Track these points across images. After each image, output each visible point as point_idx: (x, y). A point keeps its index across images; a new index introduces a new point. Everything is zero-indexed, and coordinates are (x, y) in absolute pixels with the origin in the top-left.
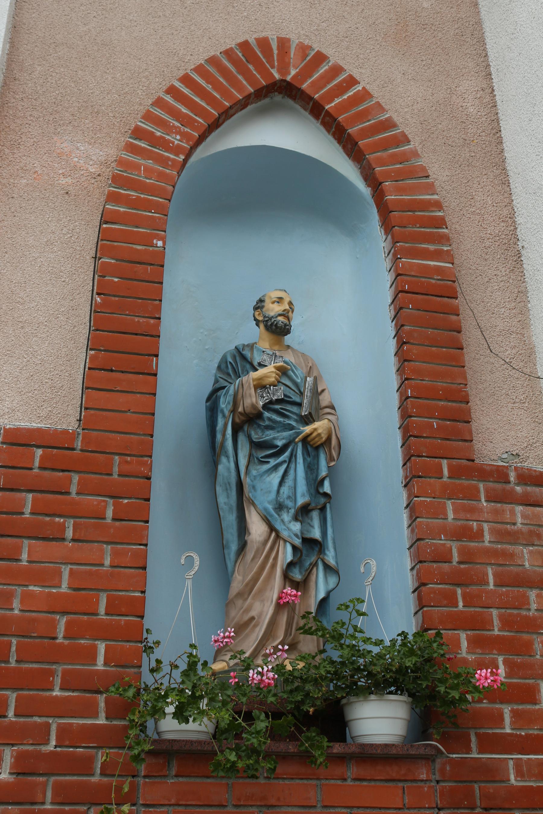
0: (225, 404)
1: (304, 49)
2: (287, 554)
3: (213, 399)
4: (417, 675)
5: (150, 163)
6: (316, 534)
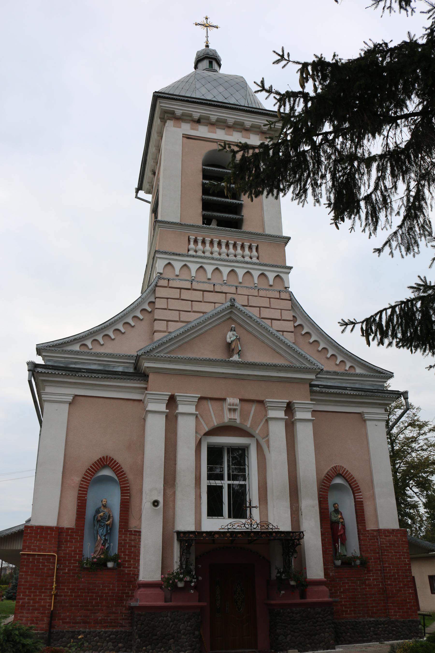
0: (96, 519)
1: (110, 458)
2: (102, 542)
3: (94, 517)
4: (114, 559)
5: (85, 483)
6: (107, 538)
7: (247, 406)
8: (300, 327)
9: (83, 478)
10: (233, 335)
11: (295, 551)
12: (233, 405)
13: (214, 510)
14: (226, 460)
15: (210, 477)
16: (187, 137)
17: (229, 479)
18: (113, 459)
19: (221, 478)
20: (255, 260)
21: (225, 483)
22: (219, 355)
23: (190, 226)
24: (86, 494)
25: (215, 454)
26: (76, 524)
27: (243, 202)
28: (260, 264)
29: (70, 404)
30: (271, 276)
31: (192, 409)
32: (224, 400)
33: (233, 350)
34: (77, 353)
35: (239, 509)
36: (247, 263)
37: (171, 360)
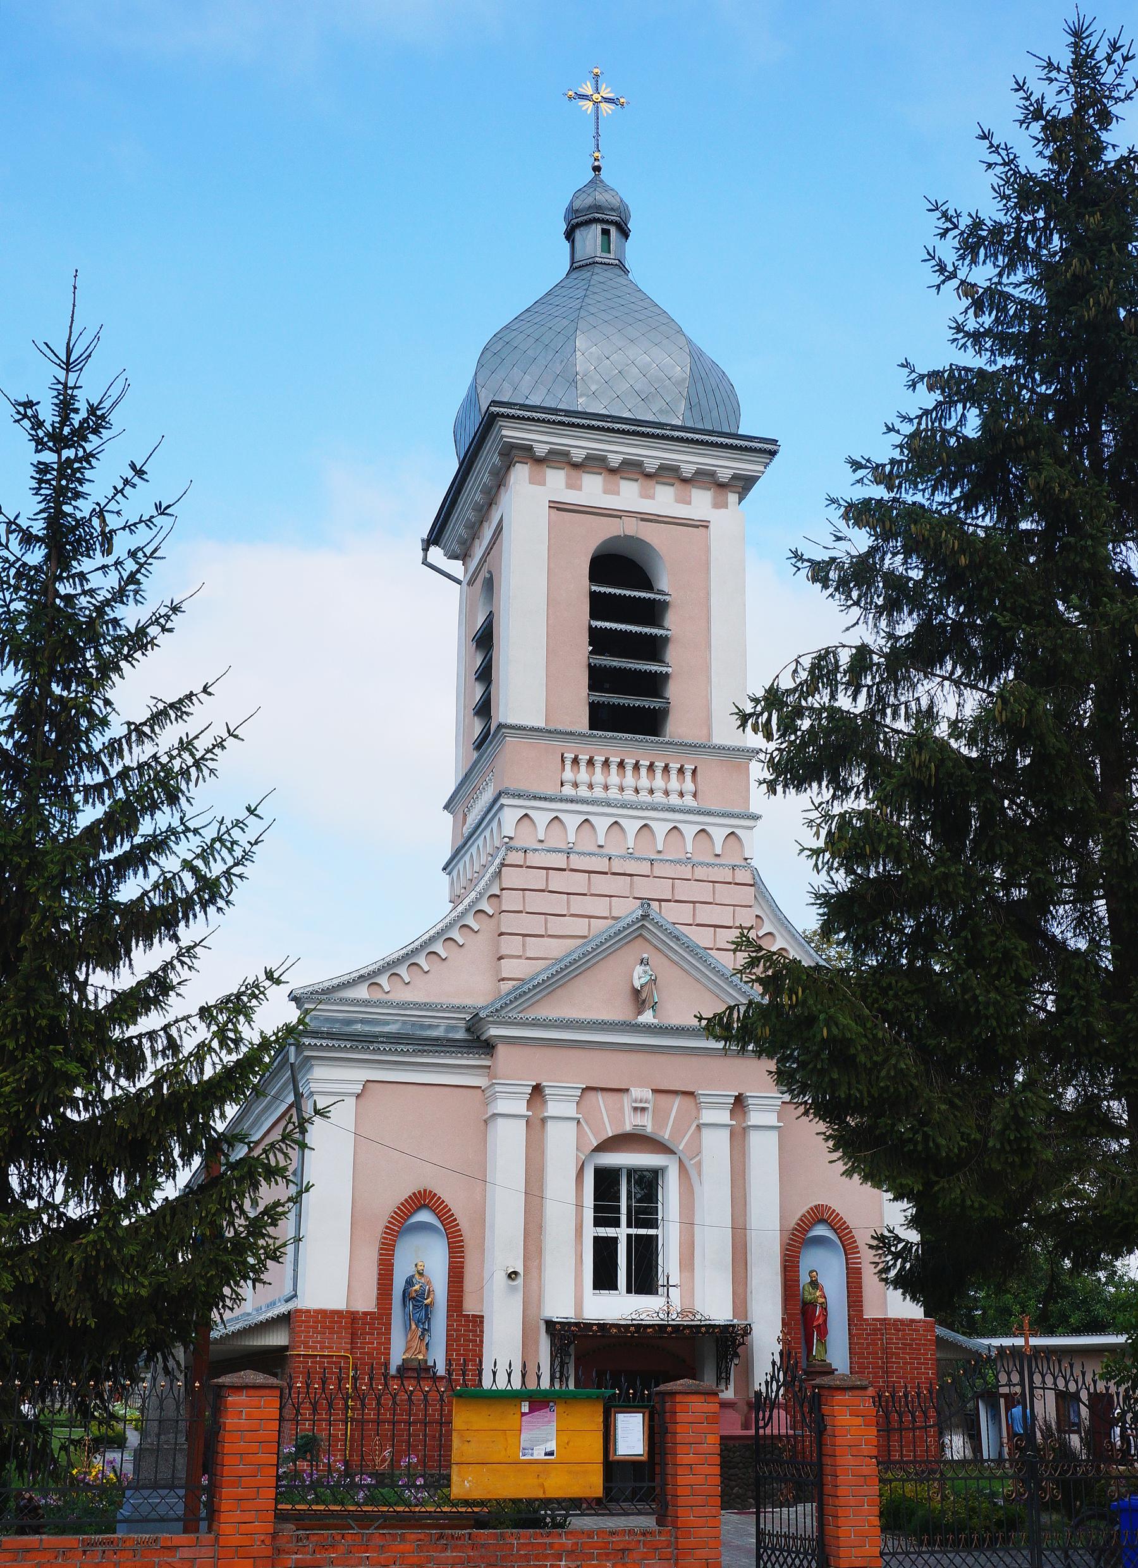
1: (431, 1192)
7: (663, 1098)
8: (769, 937)
9: (387, 1227)
10: (645, 972)
11: (737, 1355)
12: (641, 1101)
13: (604, 1279)
14: (625, 1197)
15: (598, 1223)
16: (557, 507)
17: (629, 1226)
18: (435, 1195)
19: (616, 1223)
20: (689, 801)
21: (622, 1233)
22: (620, 1011)
23: (567, 733)
24: (393, 1255)
25: (606, 1181)
26: (378, 1304)
27: (670, 669)
28: (699, 813)
29: (358, 1096)
30: (719, 834)
31: (570, 1110)
32: (627, 1090)
33: (644, 1001)
34: (366, 1003)
35: (644, 1279)
36: (673, 810)
37: (536, 1024)
